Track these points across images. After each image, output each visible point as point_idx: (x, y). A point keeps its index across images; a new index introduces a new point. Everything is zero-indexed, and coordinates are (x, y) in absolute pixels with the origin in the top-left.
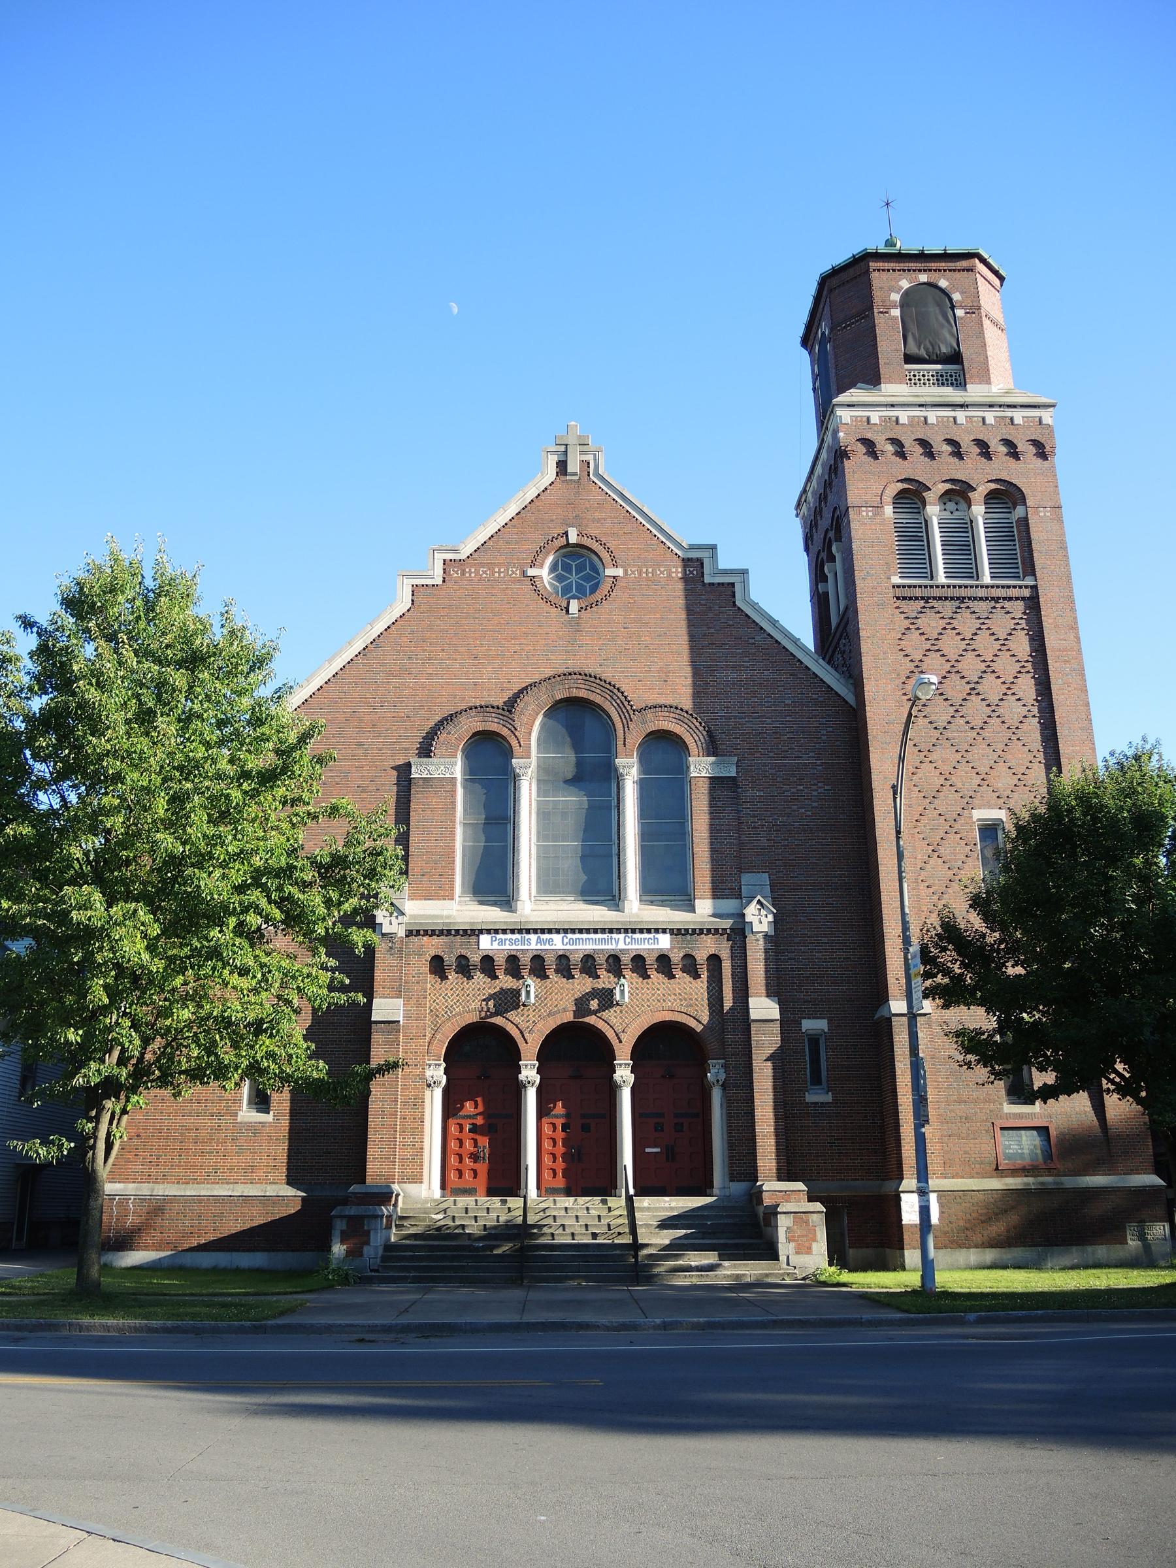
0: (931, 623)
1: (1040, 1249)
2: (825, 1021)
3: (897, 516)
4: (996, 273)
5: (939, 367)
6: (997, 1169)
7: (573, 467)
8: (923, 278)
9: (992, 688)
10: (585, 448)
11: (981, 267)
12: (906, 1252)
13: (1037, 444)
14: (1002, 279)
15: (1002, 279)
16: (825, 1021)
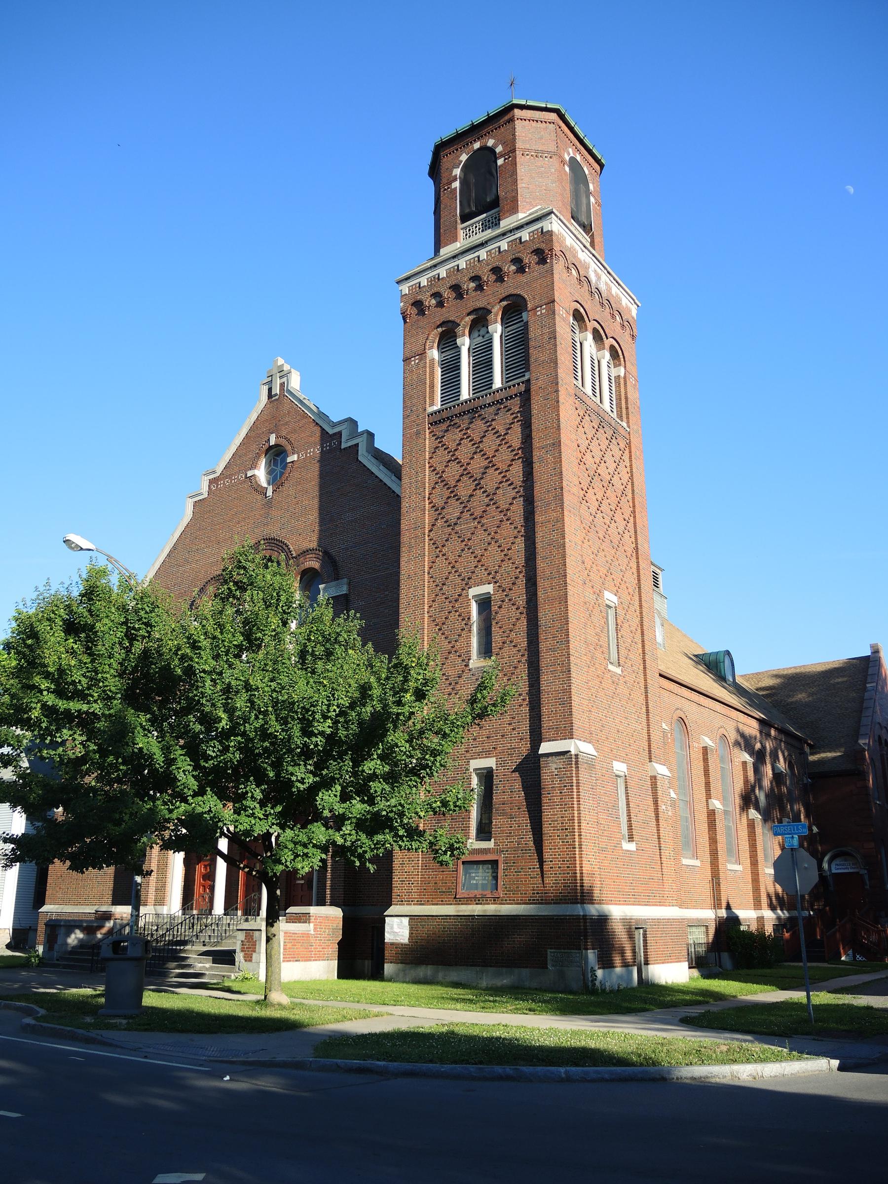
0: (452, 438)
1: (478, 968)
2: (494, 759)
3: (444, 355)
4: (598, 161)
5: (485, 215)
6: (455, 898)
7: (276, 390)
8: (477, 145)
9: (491, 480)
10: (282, 374)
11: (517, 112)
12: (386, 965)
13: (538, 252)
14: (602, 166)
15: (602, 166)
16: (494, 759)
